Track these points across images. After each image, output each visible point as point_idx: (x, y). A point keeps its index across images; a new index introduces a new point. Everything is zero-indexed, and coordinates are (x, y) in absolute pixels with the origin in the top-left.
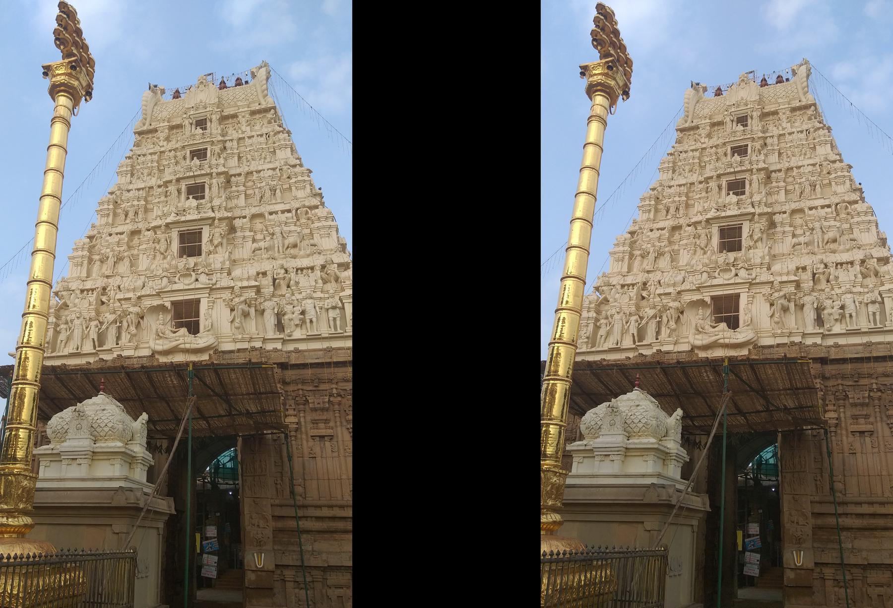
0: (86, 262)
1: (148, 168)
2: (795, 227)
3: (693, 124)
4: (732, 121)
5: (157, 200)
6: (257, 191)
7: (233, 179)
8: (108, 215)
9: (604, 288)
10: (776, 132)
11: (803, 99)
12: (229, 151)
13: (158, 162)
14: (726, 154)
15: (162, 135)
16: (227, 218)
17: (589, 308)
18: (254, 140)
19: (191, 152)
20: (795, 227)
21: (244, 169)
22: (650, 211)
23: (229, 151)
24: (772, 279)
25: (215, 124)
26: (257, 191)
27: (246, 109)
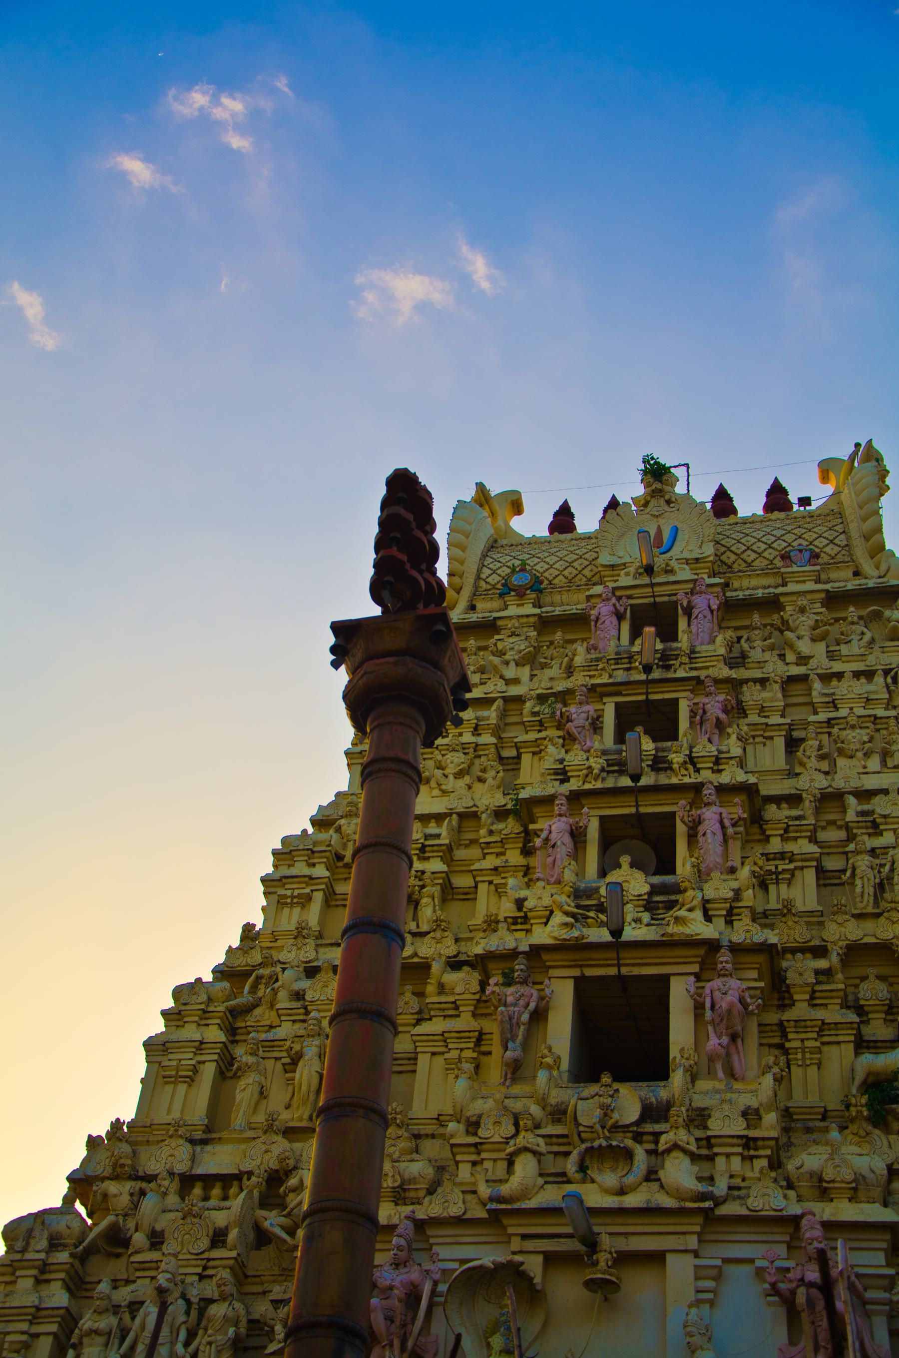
0: (209, 1071)
1: (464, 747)
2: (860, 1010)
3: (474, 617)
4: (620, 617)
5: (491, 862)
6: (863, 862)
7: (772, 812)
8: (309, 898)
9: (112, 1187)
10: (776, 668)
11: (867, 567)
12: (753, 718)
13: (497, 732)
14: (596, 726)
15: (515, 646)
16: (765, 948)
17: (44, 1267)
18: (841, 688)
19: (619, 708)
20: (860, 1010)
21: (812, 781)
22: (305, 901)
23: (753, 718)
24: (795, 1209)
25: (703, 624)
26: (863, 862)
27: (811, 586)
